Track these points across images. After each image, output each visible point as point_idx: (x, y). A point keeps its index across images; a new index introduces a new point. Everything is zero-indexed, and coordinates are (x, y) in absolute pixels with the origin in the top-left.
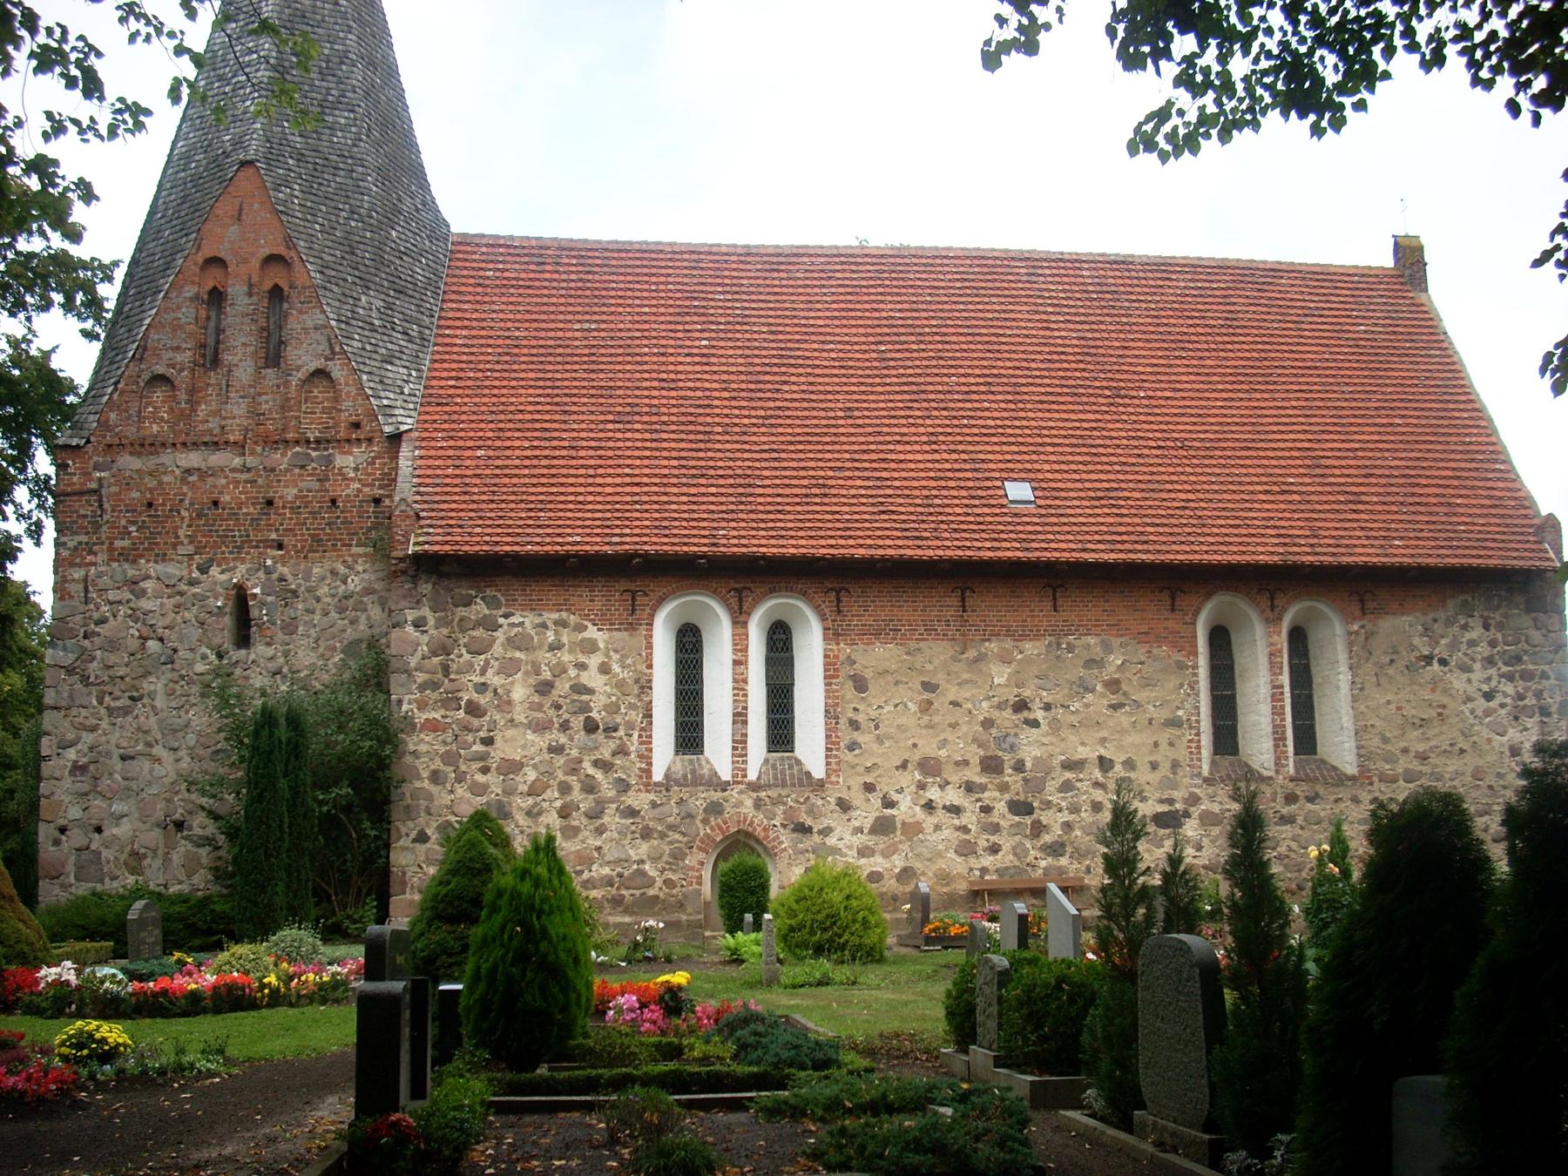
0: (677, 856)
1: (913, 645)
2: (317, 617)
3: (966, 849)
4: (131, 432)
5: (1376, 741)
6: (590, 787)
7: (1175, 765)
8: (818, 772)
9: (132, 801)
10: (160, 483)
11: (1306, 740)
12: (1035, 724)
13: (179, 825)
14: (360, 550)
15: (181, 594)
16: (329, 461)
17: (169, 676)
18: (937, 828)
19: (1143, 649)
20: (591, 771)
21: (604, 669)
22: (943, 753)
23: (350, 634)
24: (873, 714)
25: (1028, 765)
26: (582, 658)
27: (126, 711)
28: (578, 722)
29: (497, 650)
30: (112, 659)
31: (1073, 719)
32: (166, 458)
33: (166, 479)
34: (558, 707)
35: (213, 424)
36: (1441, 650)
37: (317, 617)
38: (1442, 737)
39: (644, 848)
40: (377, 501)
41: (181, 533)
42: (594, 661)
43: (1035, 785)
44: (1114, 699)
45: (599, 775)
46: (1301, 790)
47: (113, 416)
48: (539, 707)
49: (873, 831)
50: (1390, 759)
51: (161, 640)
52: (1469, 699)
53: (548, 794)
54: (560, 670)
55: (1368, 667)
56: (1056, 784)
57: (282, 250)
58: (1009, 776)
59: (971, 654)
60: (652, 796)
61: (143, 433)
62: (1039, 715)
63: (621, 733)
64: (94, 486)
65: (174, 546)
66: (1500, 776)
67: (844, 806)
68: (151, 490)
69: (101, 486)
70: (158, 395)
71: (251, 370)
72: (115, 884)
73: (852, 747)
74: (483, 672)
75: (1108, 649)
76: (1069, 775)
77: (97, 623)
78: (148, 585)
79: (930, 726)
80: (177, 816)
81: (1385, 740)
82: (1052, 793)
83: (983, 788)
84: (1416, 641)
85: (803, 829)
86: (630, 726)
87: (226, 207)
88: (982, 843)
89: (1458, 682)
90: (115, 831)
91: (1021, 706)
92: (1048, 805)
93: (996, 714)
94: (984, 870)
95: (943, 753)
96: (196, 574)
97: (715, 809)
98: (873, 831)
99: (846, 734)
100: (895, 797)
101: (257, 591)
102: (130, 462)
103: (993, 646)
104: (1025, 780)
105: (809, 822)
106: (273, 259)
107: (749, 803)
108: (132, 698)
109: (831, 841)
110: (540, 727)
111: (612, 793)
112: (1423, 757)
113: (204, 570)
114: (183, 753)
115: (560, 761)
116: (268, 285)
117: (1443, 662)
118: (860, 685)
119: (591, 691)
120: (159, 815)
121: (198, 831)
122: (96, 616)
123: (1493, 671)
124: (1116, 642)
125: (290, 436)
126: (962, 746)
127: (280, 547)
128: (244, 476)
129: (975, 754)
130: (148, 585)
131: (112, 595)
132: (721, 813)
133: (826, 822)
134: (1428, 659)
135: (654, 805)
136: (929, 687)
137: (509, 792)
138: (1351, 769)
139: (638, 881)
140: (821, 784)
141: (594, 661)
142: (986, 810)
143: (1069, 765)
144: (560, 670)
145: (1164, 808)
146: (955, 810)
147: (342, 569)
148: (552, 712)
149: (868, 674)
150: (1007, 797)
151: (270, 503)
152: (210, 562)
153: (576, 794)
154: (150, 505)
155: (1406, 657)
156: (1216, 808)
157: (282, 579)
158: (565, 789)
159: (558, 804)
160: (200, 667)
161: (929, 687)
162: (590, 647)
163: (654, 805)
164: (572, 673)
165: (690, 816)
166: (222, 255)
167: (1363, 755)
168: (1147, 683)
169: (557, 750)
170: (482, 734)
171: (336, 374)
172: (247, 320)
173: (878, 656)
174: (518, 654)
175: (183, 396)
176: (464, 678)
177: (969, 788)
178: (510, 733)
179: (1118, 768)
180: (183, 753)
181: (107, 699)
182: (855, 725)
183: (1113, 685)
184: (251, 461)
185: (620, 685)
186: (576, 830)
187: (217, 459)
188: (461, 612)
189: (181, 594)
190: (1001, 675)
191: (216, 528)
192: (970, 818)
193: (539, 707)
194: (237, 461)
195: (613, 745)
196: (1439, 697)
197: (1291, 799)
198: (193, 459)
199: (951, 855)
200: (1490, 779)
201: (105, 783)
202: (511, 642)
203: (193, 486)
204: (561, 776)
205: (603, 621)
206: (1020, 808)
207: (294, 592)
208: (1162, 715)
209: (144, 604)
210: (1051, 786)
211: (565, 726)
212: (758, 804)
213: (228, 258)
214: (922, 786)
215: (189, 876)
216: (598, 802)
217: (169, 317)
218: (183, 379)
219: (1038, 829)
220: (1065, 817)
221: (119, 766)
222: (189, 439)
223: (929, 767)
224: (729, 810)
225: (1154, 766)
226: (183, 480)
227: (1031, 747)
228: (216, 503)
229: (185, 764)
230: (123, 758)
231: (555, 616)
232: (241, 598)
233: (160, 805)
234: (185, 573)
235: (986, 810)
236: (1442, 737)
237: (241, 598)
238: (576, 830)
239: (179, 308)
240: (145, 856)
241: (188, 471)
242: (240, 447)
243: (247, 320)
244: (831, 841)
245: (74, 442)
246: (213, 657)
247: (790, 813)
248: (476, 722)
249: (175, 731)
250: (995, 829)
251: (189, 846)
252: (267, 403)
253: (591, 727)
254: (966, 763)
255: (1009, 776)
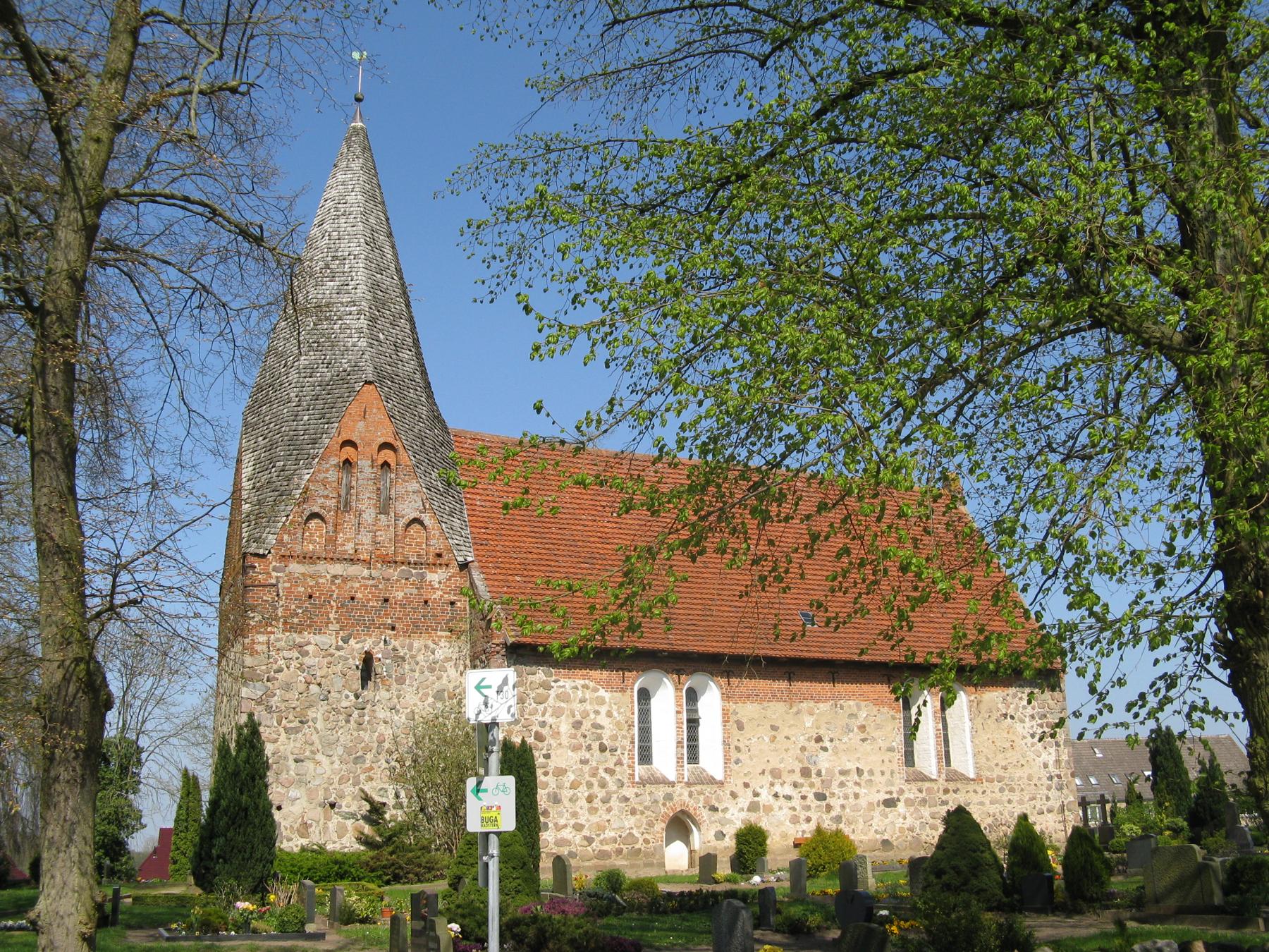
0: (651, 825)
1: (766, 704)
2: (417, 674)
3: (795, 820)
4: (298, 549)
5: (984, 760)
6: (603, 785)
7: (892, 773)
8: (719, 776)
9: (303, 789)
10: (317, 583)
11: (946, 757)
12: (825, 749)
13: (333, 806)
14: (444, 634)
15: (332, 655)
16: (422, 576)
17: (326, 708)
18: (780, 808)
19: (875, 709)
20: (603, 774)
21: (609, 714)
22: (782, 765)
23: (437, 686)
24: (747, 743)
25: (823, 772)
26: (597, 708)
27: (297, 730)
28: (596, 746)
29: (551, 701)
30: (288, 696)
31: (844, 747)
32: (322, 567)
33: (321, 581)
34: (585, 736)
35: (349, 547)
36: (1011, 711)
37: (417, 674)
38: (1012, 756)
39: (633, 819)
40: (452, 603)
41: (331, 616)
42: (603, 709)
43: (826, 783)
44: (863, 736)
45: (607, 777)
46: (951, 786)
47: (286, 537)
48: (575, 737)
49: (749, 810)
50: (990, 769)
51: (319, 685)
52: (1024, 737)
53: (581, 789)
54: (585, 715)
55: (979, 720)
56: (837, 783)
57: (391, 440)
58: (814, 779)
59: (795, 709)
60: (636, 790)
61: (305, 549)
62: (827, 744)
63: (619, 752)
64: (273, 581)
65: (327, 624)
66: (1039, 779)
67: (734, 795)
68: (311, 587)
69: (278, 582)
70: (313, 524)
71: (373, 515)
72: (291, 844)
73: (737, 762)
74: (543, 715)
75: (859, 708)
76: (843, 778)
77: (275, 672)
78: (310, 648)
79: (776, 750)
80: (332, 799)
81: (988, 759)
82: (835, 788)
83: (802, 785)
84: (1000, 706)
85: (714, 809)
86: (624, 748)
87: (355, 409)
88: (803, 817)
89: (1018, 727)
90: (291, 809)
91: (819, 739)
92: (833, 794)
93: (806, 744)
94: (804, 832)
95: (782, 765)
96: (341, 643)
97: (669, 797)
98: (749, 810)
99: (734, 755)
100: (759, 790)
101: (380, 656)
102: (295, 567)
103: (804, 705)
104: (823, 781)
105: (716, 805)
106: (385, 446)
107: (686, 794)
108: (301, 722)
109: (728, 816)
110: (576, 748)
111: (615, 788)
112: (1005, 768)
113: (346, 641)
114: (335, 758)
115: (586, 768)
116: (380, 462)
117: (1012, 717)
118: (740, 727)
119: (601, 727)
120: (320, 798)
121: (344, 809)
122: (275, 667)
123: (1034, 723)
124: (863, 704)
125: (398, 559)
126: (790, 762)
127: (393, 629)
128: (371, 582)
129: (798, 767)
130: (310, 648)
131: (287, 654)
132: (672, 799)
133: (726, 805)
134: (1005, 715)
135: (637, 795)
136: (774, 728)
137: (560, 787)
138: (972, 776)
139: (630, 840)
140: (722, 783)
141: (603, 709)
142: (804, 798)
143: (843, 773)
144: (585, 715)
145: (888, 796)
146: (788, 798)
147: (432, 646)
148: (582, 740)
149: (744, 720)
150: (814, 790)
151: (386, 600)
152: (350, 636)
153: (596, 789)
154: (310, 597)
155: (996, 715)
156: (912, 796)
157: (395, 649)
158: (590, 785)
159: (586, 794)
160: (345, 704)
161: (774, 728)
162: (601, 701)
163: (637, 795)
164: (592, 716)
165: (656, 801)
166: (354, 439)
167: (978, 767)
168: (878, 727)
169: (584, 762)
170: (544, 752)
171: (426, 522)
172: (370, 482)
173: (748, 710)
174: (562, 705)
175: (331, 528)
176: (533, 718)
177: (795, 785)
178: (559, 752)
179: (866, 774)
180: (335, 758)
181: (284, 721)
182: (738, 749)
183: (862, 728)
184: (374, 573)
185: (618, 724)
186: (596, 809)
187: (353, 570)
188: (531, 678)
189: (332, 655)
190: (809, 722)
191: (353, 614)
192: (796, 802)
193: (575, 737)
194: (366, 573)
195: (614, 759)
196: (1011, 737)
197: (946, 791)
198: (337, 569)
199: (788, 823)
200: (1035, 781)
201: (284, 776)
202: (558, 696)
203: (339, 587)
204: (588, 778)
205: (608, 686)
206: (820, 797)
207: (403, 658)
208: (884, 745)
209: (307, 661)
210: (835, 784)
211: (589, 748)
212: (691, 795)
213: (358, 442)
214: (772, 784)
215: (340, 837)
216: (607, 793)
217: (322, 476)
218: (330, 516)
219: (829, 808)
220: (841, 801)
221: (292, 764)
222: (337, 556)
223: (776, 774)
224: (676, 798)
225: (883, 773)
226: (332, 582)
227: (824, 762)
228: (353, 598)
229: (337, 765)
230: (296, 761)
231: (582, 682)
232: (368, 660)
233: (321, 793)
234: (334, 642)
235: (804, 798)
236: (1012, 756)
237: (368, 660)
238: (596, 809)
239: (327, 470)
240: (311, 825)
241: (335, 577)
242: (367, 563)
243: (370, 482)
244: (728, 816)
245: (261, 552)
246: (352, 697)
247: (707, 801)
248: (540, 745)
249: (330, 744)
250: (808, 808)
251: (340, 819)
252: (382, 536)
253: (603, 749)
254: (793, 771)
255: (814, 779)
